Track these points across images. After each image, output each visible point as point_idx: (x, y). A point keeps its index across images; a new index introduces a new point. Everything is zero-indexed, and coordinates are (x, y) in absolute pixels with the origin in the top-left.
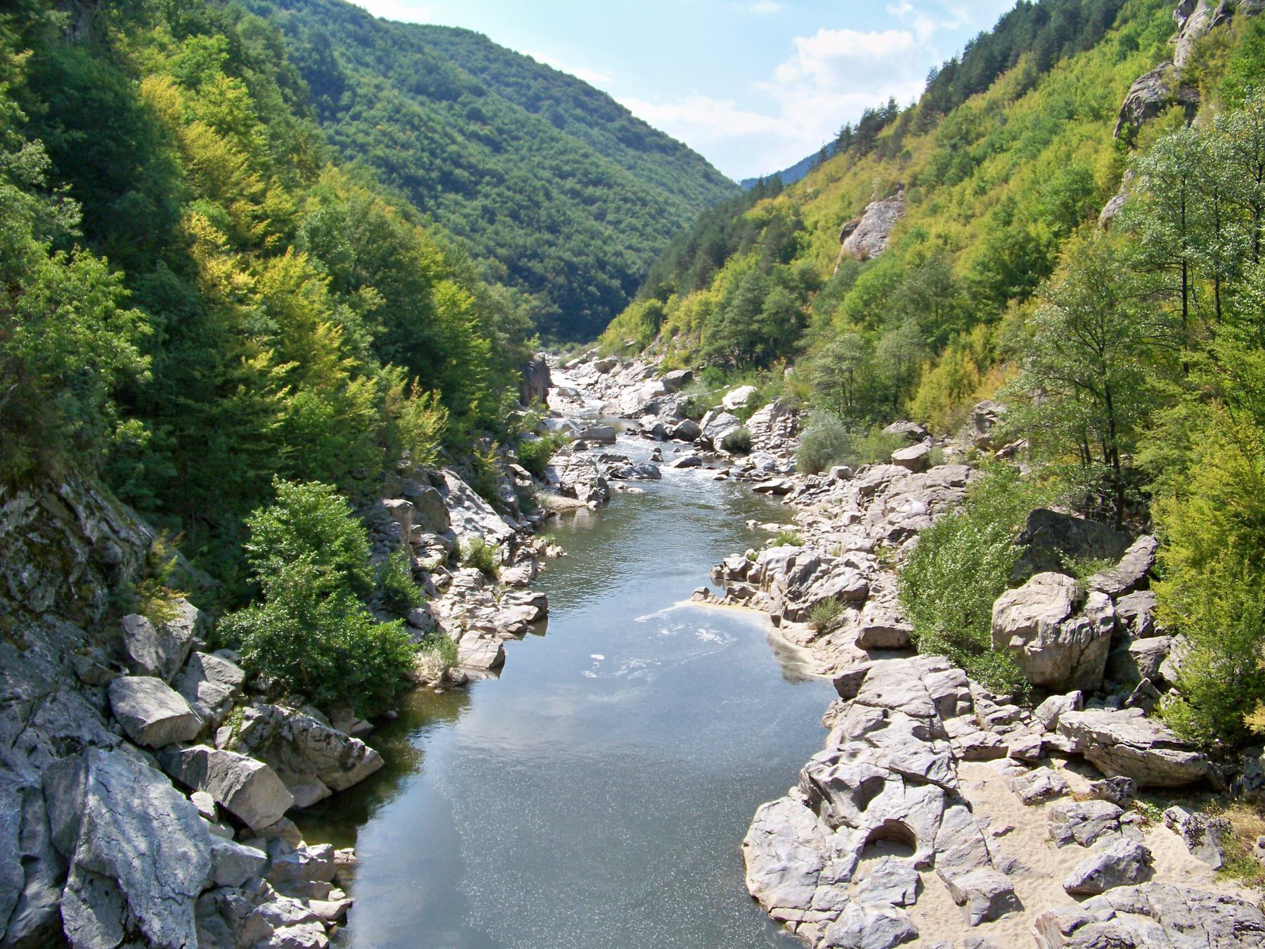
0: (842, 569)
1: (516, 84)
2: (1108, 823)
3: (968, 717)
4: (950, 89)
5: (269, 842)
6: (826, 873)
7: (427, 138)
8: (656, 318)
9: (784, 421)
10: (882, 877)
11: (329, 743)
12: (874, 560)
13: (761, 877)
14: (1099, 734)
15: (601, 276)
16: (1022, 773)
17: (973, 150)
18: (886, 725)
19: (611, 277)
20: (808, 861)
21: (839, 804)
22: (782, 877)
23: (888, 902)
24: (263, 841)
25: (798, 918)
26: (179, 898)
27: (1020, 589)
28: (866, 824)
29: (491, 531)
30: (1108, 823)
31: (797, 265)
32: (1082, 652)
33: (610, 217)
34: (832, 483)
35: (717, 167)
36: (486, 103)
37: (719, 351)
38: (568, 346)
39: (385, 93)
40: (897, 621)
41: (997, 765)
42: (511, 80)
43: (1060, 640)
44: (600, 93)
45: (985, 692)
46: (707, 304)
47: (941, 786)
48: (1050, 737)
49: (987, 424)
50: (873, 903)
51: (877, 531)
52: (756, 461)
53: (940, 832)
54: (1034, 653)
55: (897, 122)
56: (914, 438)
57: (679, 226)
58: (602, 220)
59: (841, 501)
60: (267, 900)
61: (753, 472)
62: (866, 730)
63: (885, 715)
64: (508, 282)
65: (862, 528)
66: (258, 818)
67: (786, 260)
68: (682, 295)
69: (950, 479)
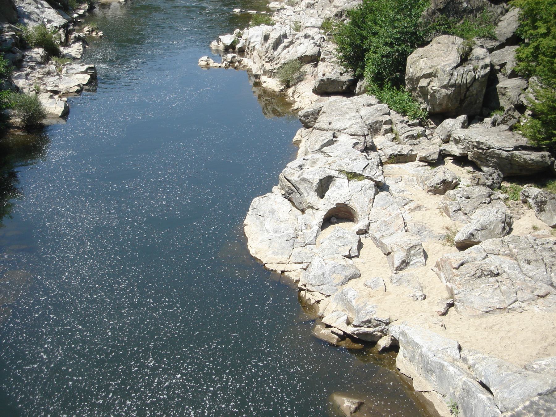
3: (389, 135)
40: (341, 74)
47: (372, 180)
48: (446, 147)
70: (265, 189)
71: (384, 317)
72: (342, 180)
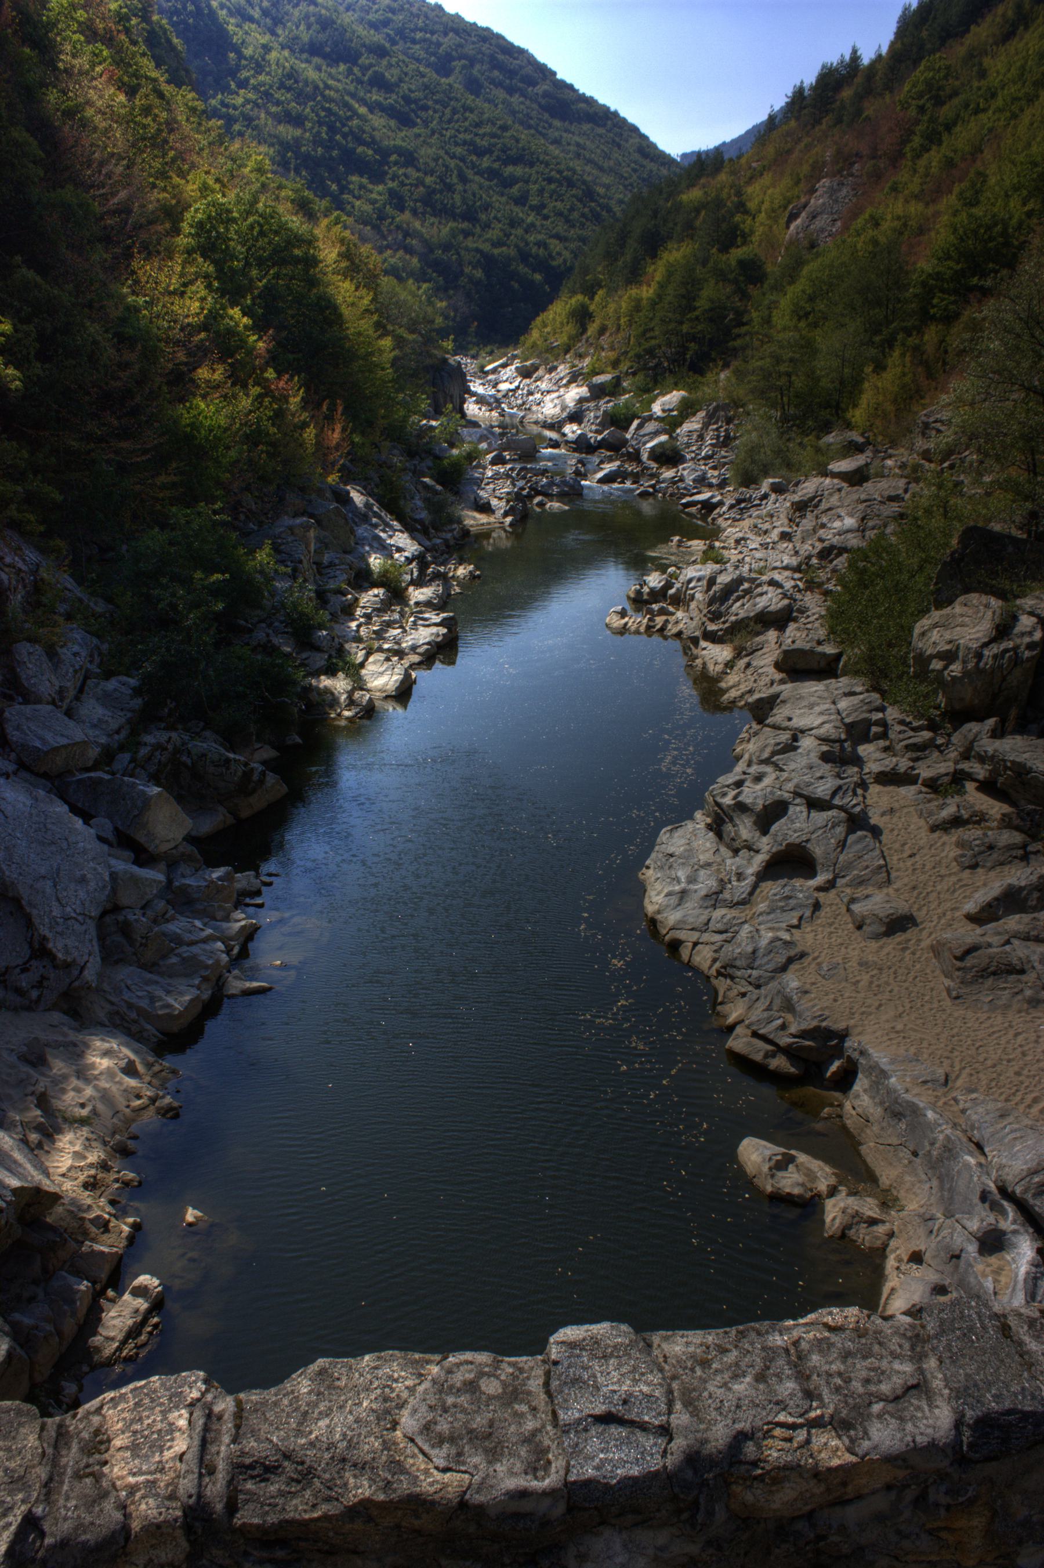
0: (765, 588)
1: (425, 40)
2: (1014, 853)
3: (882, 743)
4: (924, 34)
5: (169, 866)
6: (726, 895)
7: (324, 109)
8: (582, 317)
9: (717, 430)
10: (780, 900)
11: (228, 769)
12: (800, 579)
13: (659, 899)
14: (1013, 762)
15: (522, 269)
16: (929, 801)
17: (946, 112)
18: (796, 748)
19: (534, 271)
20: (706, 883)
21: (741, 827)
22: (681, 899)
23: (784, 925)
24: (163, 866)
25: (694, 939)
26: (80, 918)
27: (948, 610)
28: (767, 848)
29: (399, 550)
30: (1014, 853)
31: (737, 253)
32: (1004, 679)
33: (534, 201)
34: (765, 497)
35: (653, 139)
36: (390, 66)
37: (650, 352)
38: (488, 349)
39: (273, 55)
40: (819, 643)
41: (908, 792)
42: (419, 35)
43: (981, 665)
44: (522, 52)
45: (901, 717)
46: (638, 300)
47: (846, 811)
48: (965, 766)
49: (934, 433)
50: (769, 925)
51: (806, 548)
52: (685, 473)
53: (841, 858)
54: (954, 678)
55: (859, 80)
56: (852, 448)
57: (609, 210)
58: (524, 205)
59: (772, 516)
60: (168, 921)
61: (681, 485)
62: (774, 753)
63: (795, 738)
64: (421, 277)
65: (791, 546)
66: (157, 842)
67: (725, 249)
68: (612, 291)
69: (886, 494)
70: (680, 816)
71: (841, 1026)
72: (798, 808)
